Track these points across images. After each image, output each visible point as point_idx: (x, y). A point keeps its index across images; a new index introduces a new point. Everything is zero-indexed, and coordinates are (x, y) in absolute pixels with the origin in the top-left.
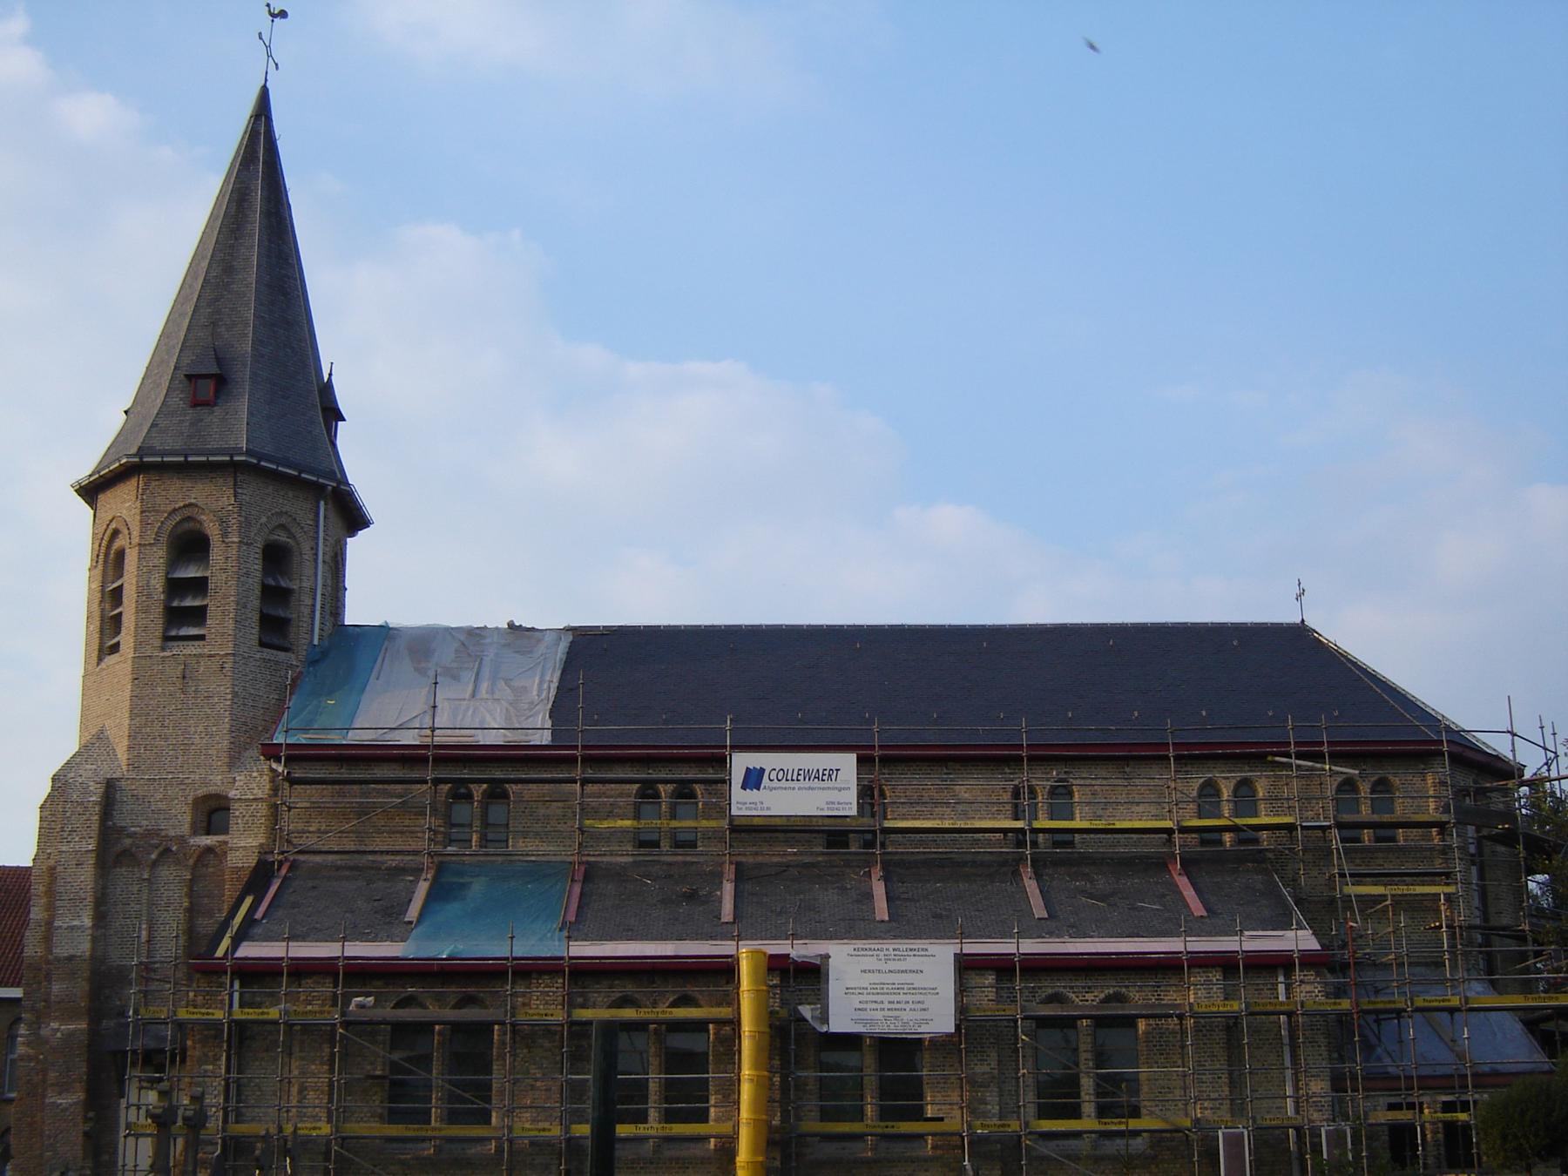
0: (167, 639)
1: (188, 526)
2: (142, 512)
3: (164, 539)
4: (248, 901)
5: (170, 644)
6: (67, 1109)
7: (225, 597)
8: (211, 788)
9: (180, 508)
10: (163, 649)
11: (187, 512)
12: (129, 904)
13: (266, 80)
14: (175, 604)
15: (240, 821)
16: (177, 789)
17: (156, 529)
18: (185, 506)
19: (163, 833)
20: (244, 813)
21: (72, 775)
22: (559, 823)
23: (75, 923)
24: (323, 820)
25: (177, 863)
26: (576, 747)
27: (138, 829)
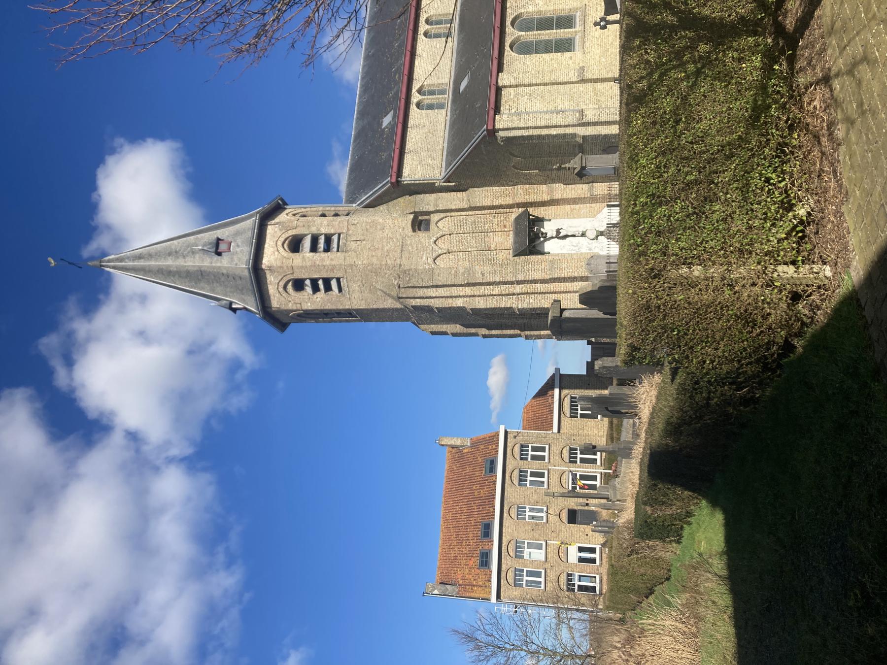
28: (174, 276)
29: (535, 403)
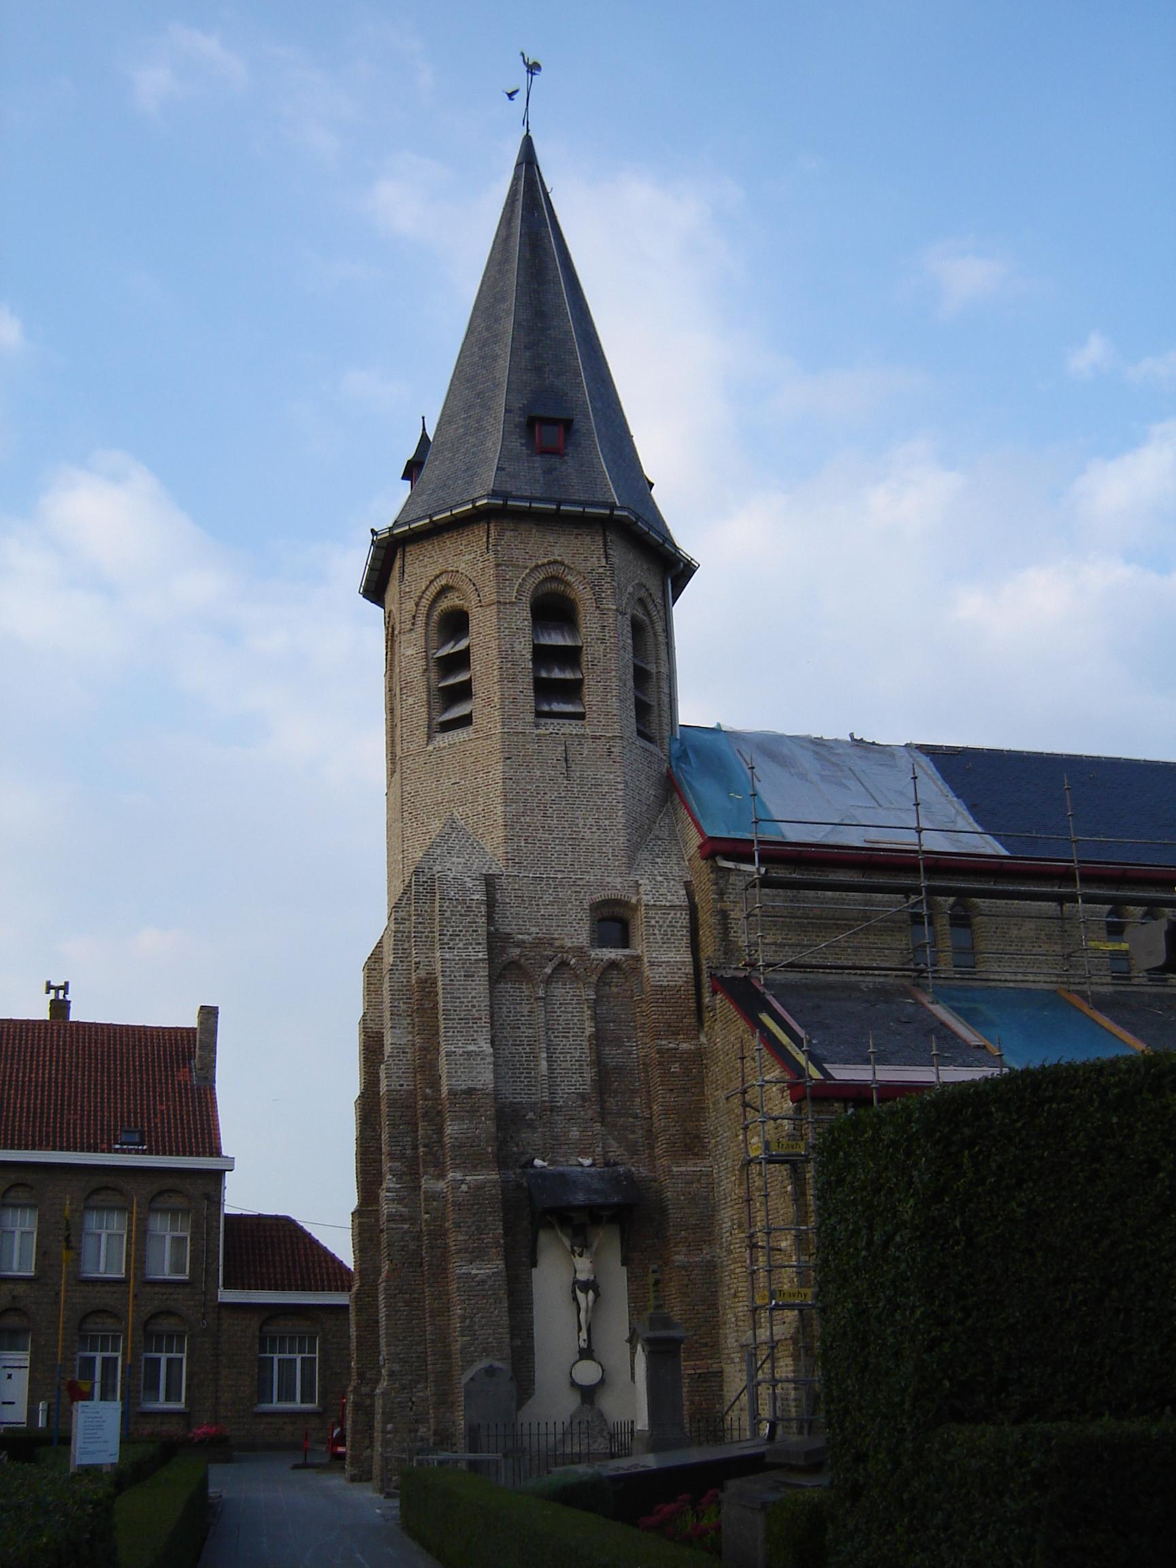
0: (539, 714)
1: (554, 586)
2: (498, 565)
3: (526, 600)
4: (766, 1018)
5: (543, 721)
6: (483, 1282)
7: (606, 671)
8: (610, 892)
9: (543, 565)
10: (537, 726)
11: (551, 570)
12: (519, 1028)
14: (544, 674)
15: (656, 932)
16: (569, 892)
17: (516, 587)
18: (549, 563)
19: (557, 943)
20: (661, 923)
21: (439, 868)
22: (1034, 947)
23: (471, 1048)
24: (779, 932)
26: (1072, 861)
27: (526, 937)
28: (488, 329)
29: (301, 1246)
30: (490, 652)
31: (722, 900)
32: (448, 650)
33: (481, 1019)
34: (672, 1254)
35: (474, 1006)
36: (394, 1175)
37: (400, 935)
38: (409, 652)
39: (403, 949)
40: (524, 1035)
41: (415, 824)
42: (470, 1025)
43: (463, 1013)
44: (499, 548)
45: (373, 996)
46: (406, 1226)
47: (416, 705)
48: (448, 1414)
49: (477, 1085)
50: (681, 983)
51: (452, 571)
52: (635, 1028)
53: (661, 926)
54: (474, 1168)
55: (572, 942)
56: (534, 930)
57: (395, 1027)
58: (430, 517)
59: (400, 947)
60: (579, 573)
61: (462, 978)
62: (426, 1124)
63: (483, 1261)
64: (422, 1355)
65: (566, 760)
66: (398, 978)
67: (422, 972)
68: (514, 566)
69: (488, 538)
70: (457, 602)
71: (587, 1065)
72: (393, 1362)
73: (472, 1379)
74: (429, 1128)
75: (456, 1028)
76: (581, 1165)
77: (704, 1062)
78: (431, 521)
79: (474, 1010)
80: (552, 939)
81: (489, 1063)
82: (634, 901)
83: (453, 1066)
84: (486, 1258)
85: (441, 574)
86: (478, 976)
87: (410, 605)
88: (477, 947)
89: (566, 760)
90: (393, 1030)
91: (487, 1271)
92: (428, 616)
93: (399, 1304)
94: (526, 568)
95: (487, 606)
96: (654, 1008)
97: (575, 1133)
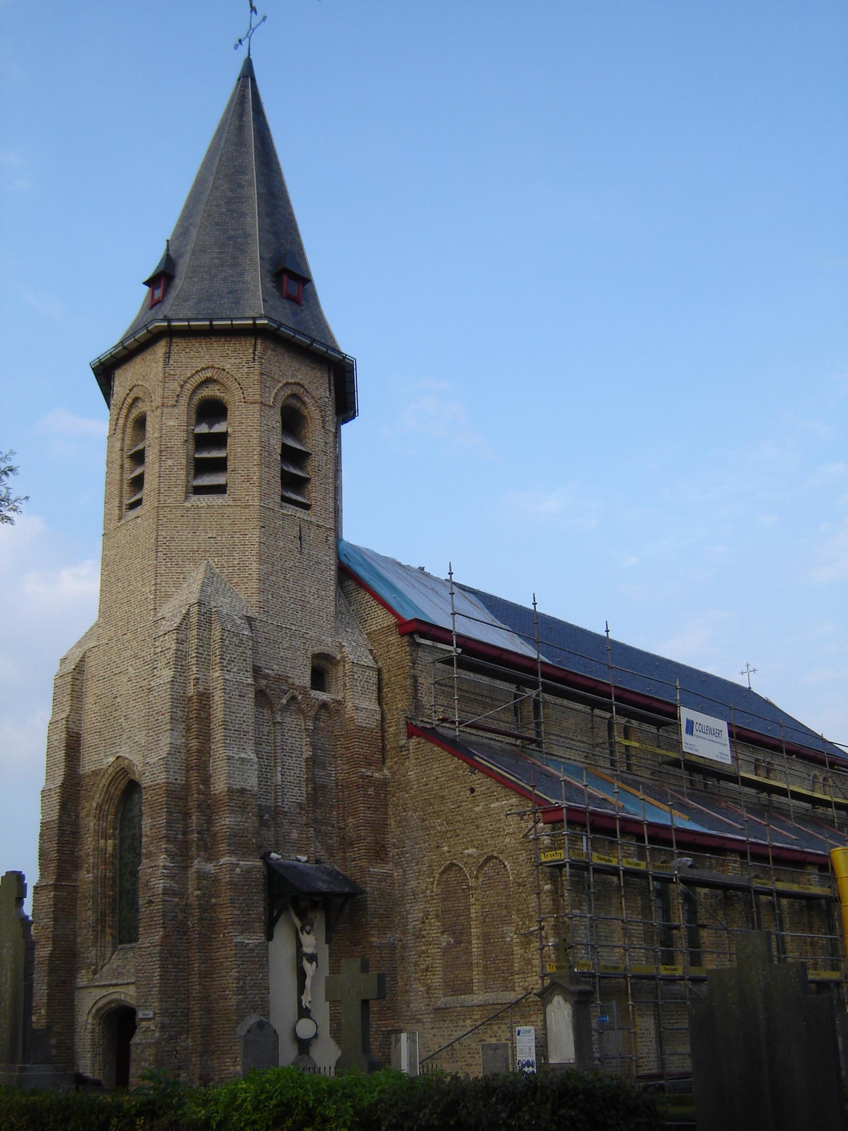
0: (284, 499)
1: (294, 401)
3: (279, 406)
9: (291, 384)
12: (261, 744)
13: (249, 54)
15: (358, 684)
19: (290, 681)
23: (243, 755)
25: (300, 711)
27: (271, 672)
30: (251, 440)
31: (414, 668)
32: (203, 429)
33: (248, 732)
34: (370, 936)
35: (244, 721)
36: (168, 856)
37: (180, 653)
38: (171, 423)
39: (181, 665)
40: (264, 750)
41: (169, 564)
42: (242, 736)
43: (237, 726)
44: (263, 361)
45: (76, 702)
46: (176, 900)
47: (175, 468)
48: (210, 1062)
49: (246, 786)
50: (373, 727)
51: (219, 369)
52: (334, 757)
53: (361, 680)
54: (244, 855)
55: (300, 682)
56: (276, 667)
57: (173, 730)
58: (211, 320)
59: (180, 663)
60: (313, 397)
61: (237, 697)
62: (199, 814)
63: (250, 933)
64: (185, 1011)
65: (300, 539)
66: (177, 689)
67: (200, 686)
68: (272, 378)
69: (255, 350)
70: (218, 394)
71: (304, 781)
72: (164, 1016)
73: (249, 1031)
74: (201, 817)
75: (232, 737)
76: (299, 861)
77: (388, 789)
78: (211, 325)
79: (245, 724)
80: (287, 677)
81: (255, 770)
82: (338, 657)
83: (232, 768)
84: (252, 930)
85: (133, 387)
86: (248, 698)
87: (175, 386)
88: (246, 673)
89: (300, 539)
90: (172, 732)
91: (255, 941)
92: (191, 398)
93: (169, 966)
94: (280, 382)
95: (250, 403)
96: (357, 743)
97: (295, 835)
